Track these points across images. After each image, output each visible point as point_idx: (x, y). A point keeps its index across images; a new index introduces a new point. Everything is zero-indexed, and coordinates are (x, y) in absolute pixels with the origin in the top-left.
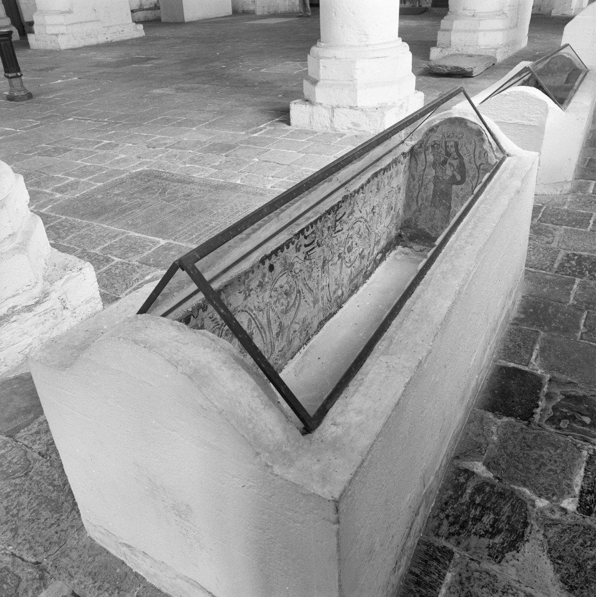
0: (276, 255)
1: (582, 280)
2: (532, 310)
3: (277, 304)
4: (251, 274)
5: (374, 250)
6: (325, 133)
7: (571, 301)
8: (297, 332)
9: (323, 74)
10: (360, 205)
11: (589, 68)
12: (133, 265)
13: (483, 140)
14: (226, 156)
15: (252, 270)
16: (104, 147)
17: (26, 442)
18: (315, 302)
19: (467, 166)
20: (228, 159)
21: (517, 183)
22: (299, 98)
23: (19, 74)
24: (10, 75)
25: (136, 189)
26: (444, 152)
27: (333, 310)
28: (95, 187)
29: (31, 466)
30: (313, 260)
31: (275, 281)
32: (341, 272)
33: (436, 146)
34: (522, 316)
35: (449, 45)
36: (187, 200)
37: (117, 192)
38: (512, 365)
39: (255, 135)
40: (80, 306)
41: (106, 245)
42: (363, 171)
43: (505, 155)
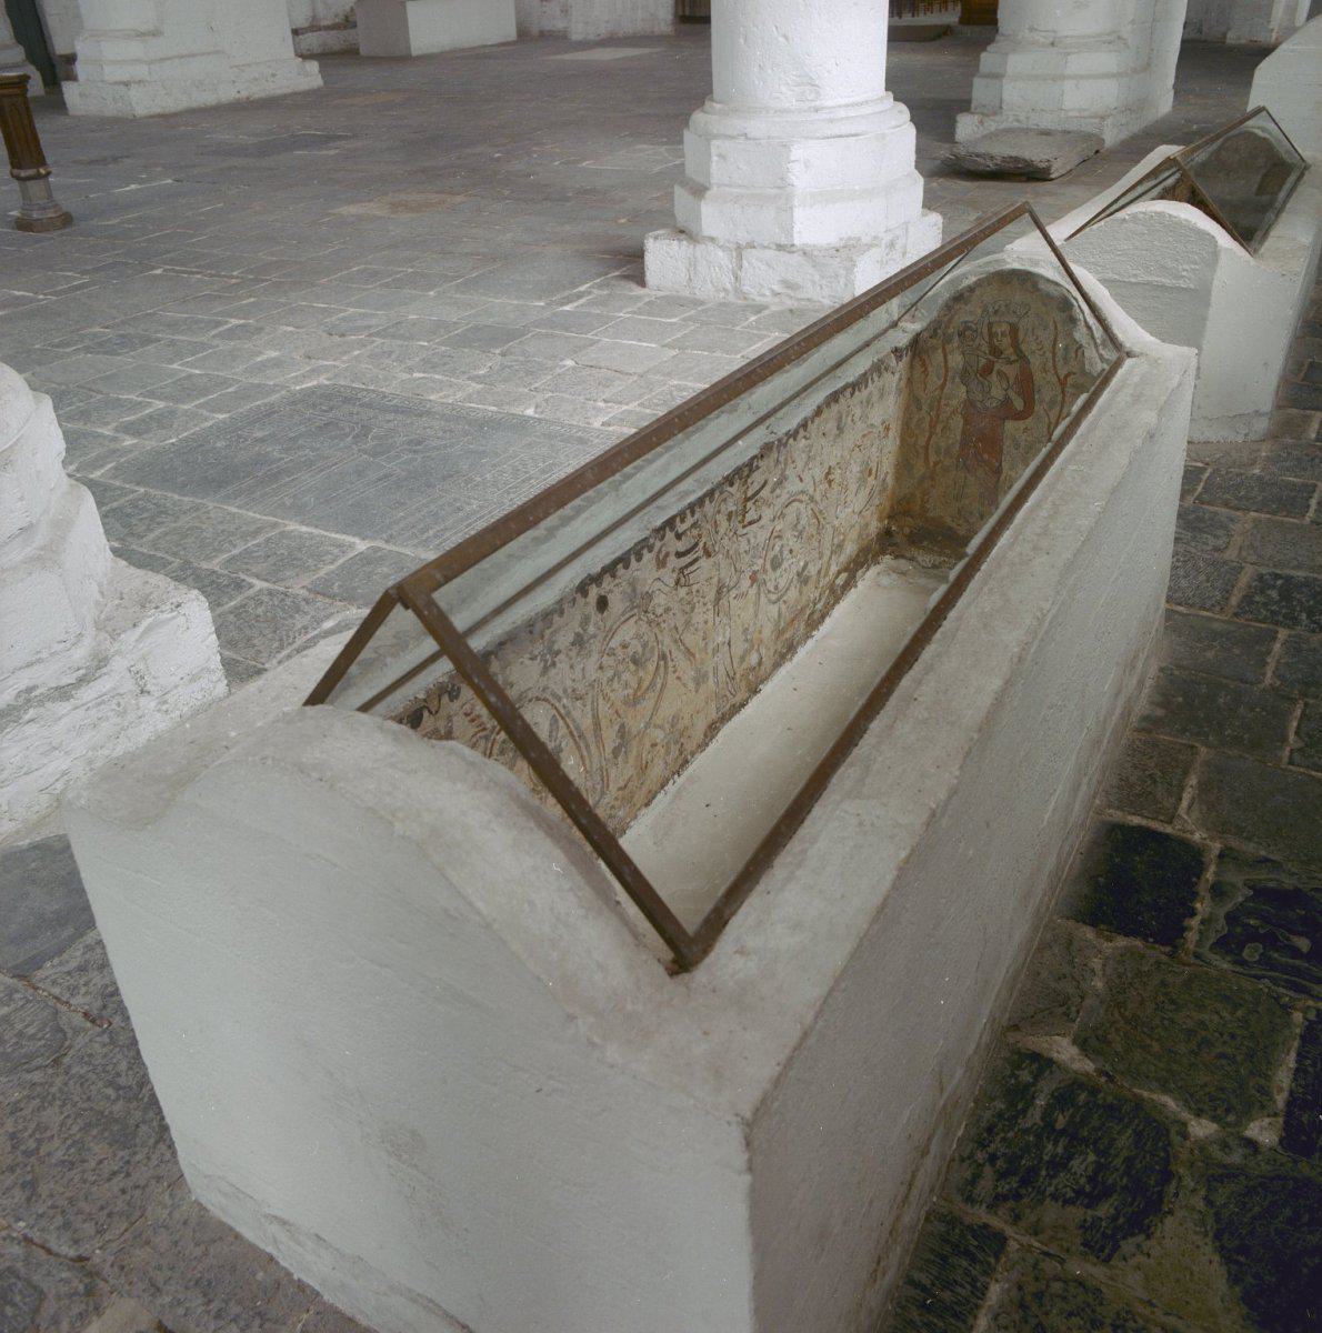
2: (1180, 699)
3: (616, 685)
5: (829, 565)
7: (1269, 678)
8: (659, 747)
9: (717, 171)
10: (800, 464)
13: (1073, 320)
15: (559, 608)
16: (231, 334)
17: (56, 991)
18: (700, 679)
19: (1038, 377)
21: (1149, 417)
23: (42, 171)
24: (23, 174)
26: (985, 348)
28: (211, 423)
29: (67, 1043)
30: (695, 587)
31: (611, 633)
34: (1160, 712)
35: (998, 109)
37: (260, 434)
38: (1136, 820)
39: (567, 308)
41: (235, 552)
42: (805, 389)
43: (1122, 353)
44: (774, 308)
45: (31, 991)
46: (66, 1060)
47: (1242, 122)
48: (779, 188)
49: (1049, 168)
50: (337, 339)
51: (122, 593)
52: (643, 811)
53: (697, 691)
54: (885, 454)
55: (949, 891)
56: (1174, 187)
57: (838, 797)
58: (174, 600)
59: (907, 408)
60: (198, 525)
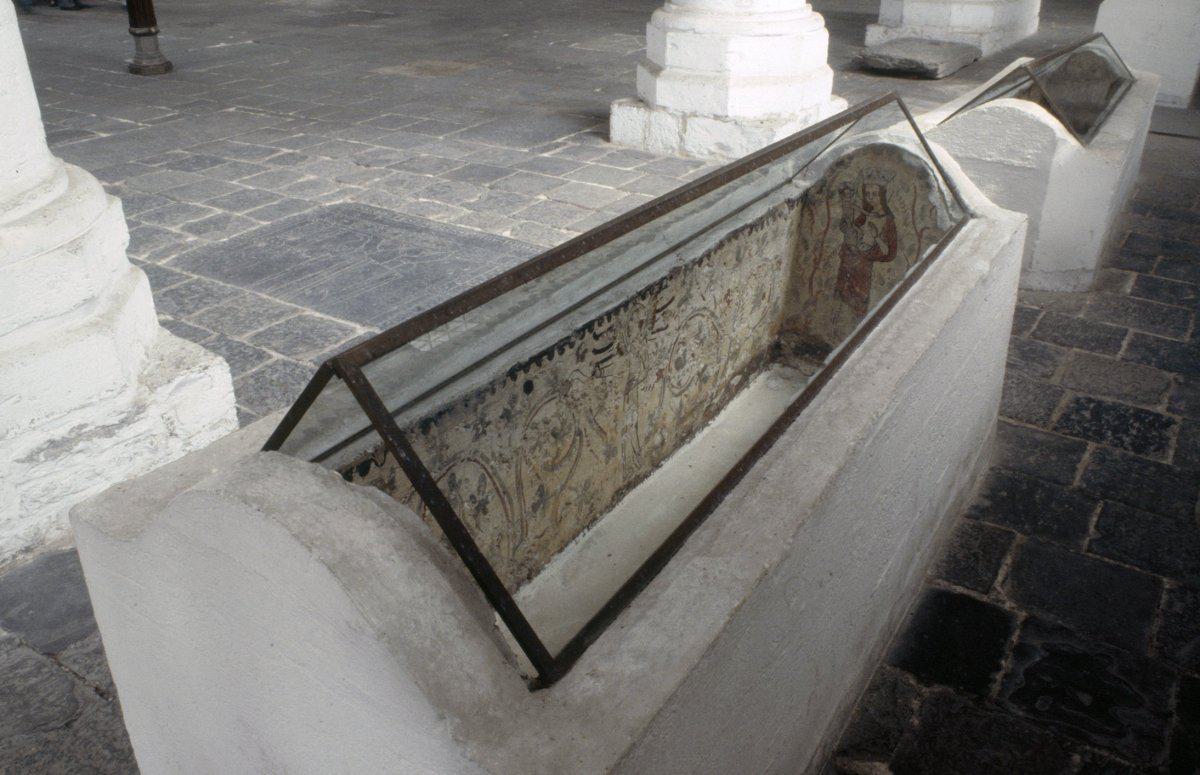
0: (539, 365)
1: (1100, 446)
2: (1005, 494)
3: (537, 453)
4: (488, 396)
5: (725, 368)
6: (668, 159)
7: (1077, 482)
8: (572, 506)
9: (671, 57)
10: (703, 286)
11: (1136, 77)
12: (304, 368)
13: (929, 186)
14: (491, 188)
15: (491, 388)
16: (282, 160)
17: (76, 668)
18: (610, 453)
19: (901, 229)
20: (493, 193)
21: (982, 266)
22: (626, 95)
23: (153, 30)
24: (138, 31)
25: (327, 236)
26: (860, 203)
27: (643, 470)
28: (258, 227)
29: (78, 711)
30: (609, 379)
31: (535, 410)
32: (661, 403)
33: (846, 191)
34: (987, 503)
35: (899, 23)
36: (413, 259)
37: (292, 239)
38: (959, 589)
39: (546, 155)
40: (199, 432)
41: (261, 329)
42: (712, 226)
43: (966, 214)
44: (709, 164)
45: (56, 666)
46: (76, 725)
47: (1081, 44)
48: (718, 72)
49: (936, 70)
50: (363, 168)
51: (163, 356)
52: (556, 557)
53: (607, 463)
54: (777, 283)
55: (781, 637)
56: (1029, 90)
57: (691, 554)
58: (202, 364)
59: (797, 247)
60: (236, 307)
